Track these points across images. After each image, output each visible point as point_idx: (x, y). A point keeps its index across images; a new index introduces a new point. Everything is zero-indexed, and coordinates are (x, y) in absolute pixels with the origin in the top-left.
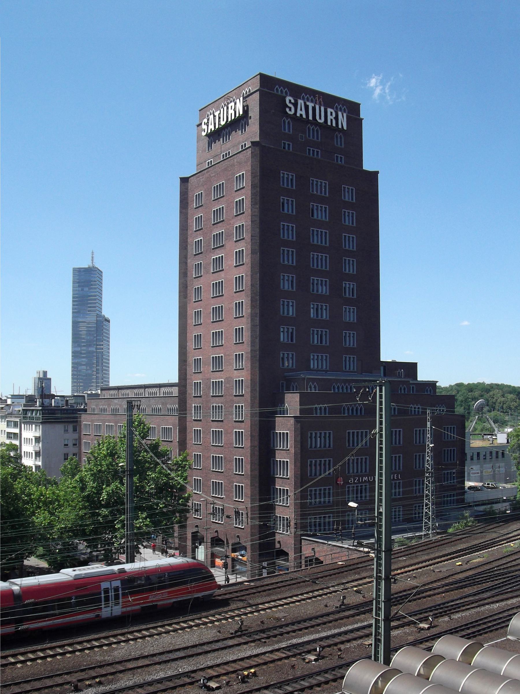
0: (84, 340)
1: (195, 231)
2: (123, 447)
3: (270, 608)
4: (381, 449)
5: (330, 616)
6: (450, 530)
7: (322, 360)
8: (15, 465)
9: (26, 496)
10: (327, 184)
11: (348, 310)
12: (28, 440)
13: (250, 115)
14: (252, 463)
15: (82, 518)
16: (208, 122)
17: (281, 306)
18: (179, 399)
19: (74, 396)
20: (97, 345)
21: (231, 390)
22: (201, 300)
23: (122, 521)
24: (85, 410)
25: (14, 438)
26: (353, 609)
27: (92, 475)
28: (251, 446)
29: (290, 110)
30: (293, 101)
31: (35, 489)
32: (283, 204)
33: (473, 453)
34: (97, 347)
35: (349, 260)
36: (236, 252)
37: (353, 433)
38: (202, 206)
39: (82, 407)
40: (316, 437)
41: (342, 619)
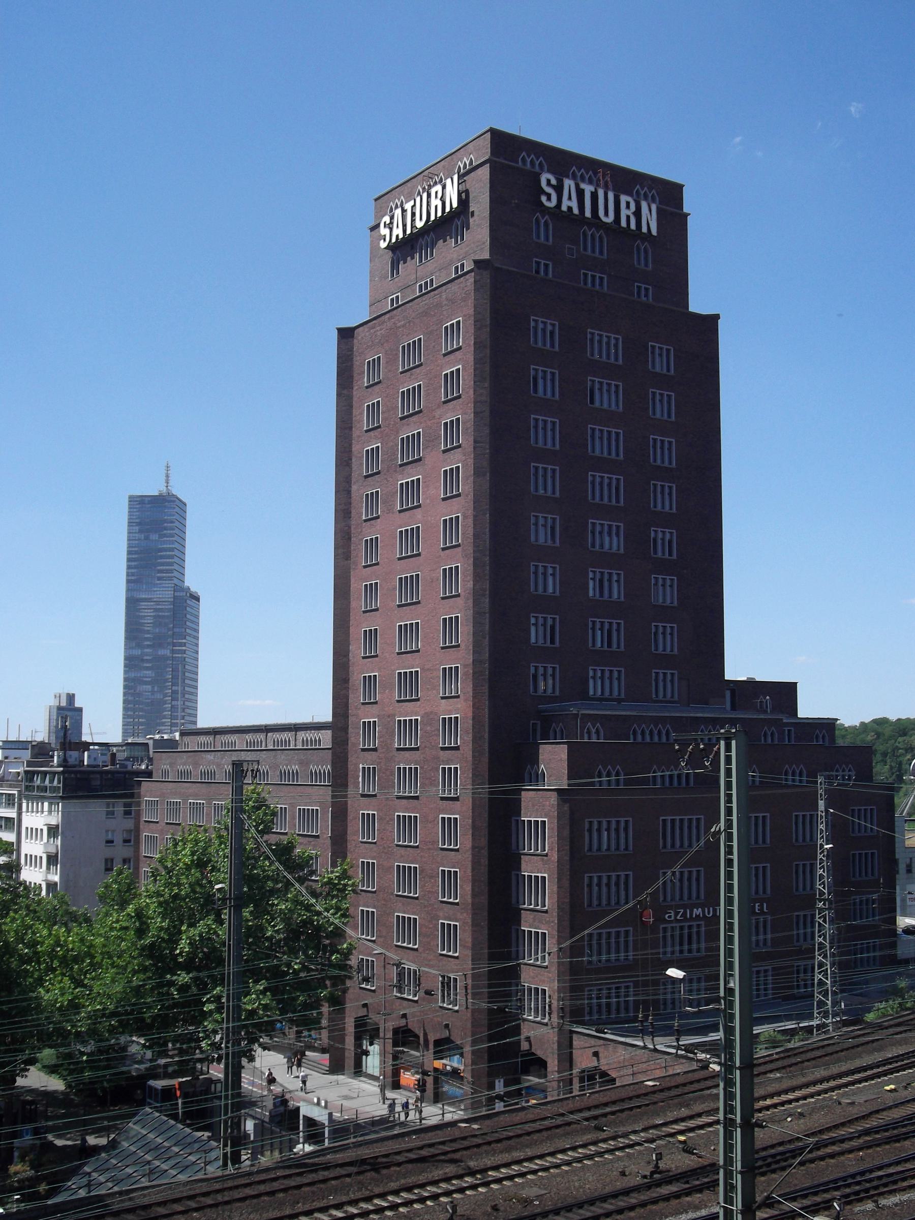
0: (148, 636)
1: (367, 431)
2: (223, 850)
3: (511, 1178)
4: (729, 863)
5: (632, 1195)
6: (870, 1017)
7: (611, 678)
8: (7, 884)
9: (27, 946)
10: (621, 340)
11: (660, 582)
12: (34, 833)
13: (471, 209)
14: (474, 881)
15: (138, 991)
16: (391, 223)
17: (532, 576)
18: (334, 754)
19: (128, 744)
20: (174, 645)
21: (435, 738)
22: (377, 564)
23: (218, 998)
24: (148, 774)
25: (6, 828)
26: (677, 1180)
27: (160, 904)
28: (473, 848)
29: (549, 199)
30: (554, 182)
31: (45, 932)
32: (535, 379)
33: (911, 859)
34: (174, 648)
35: (662, 486)
36: (446, 471)
37: (673, 821)
38: (379, 382)
39: (143, 767)
40: (599, 830)
41: (655, 1202)
